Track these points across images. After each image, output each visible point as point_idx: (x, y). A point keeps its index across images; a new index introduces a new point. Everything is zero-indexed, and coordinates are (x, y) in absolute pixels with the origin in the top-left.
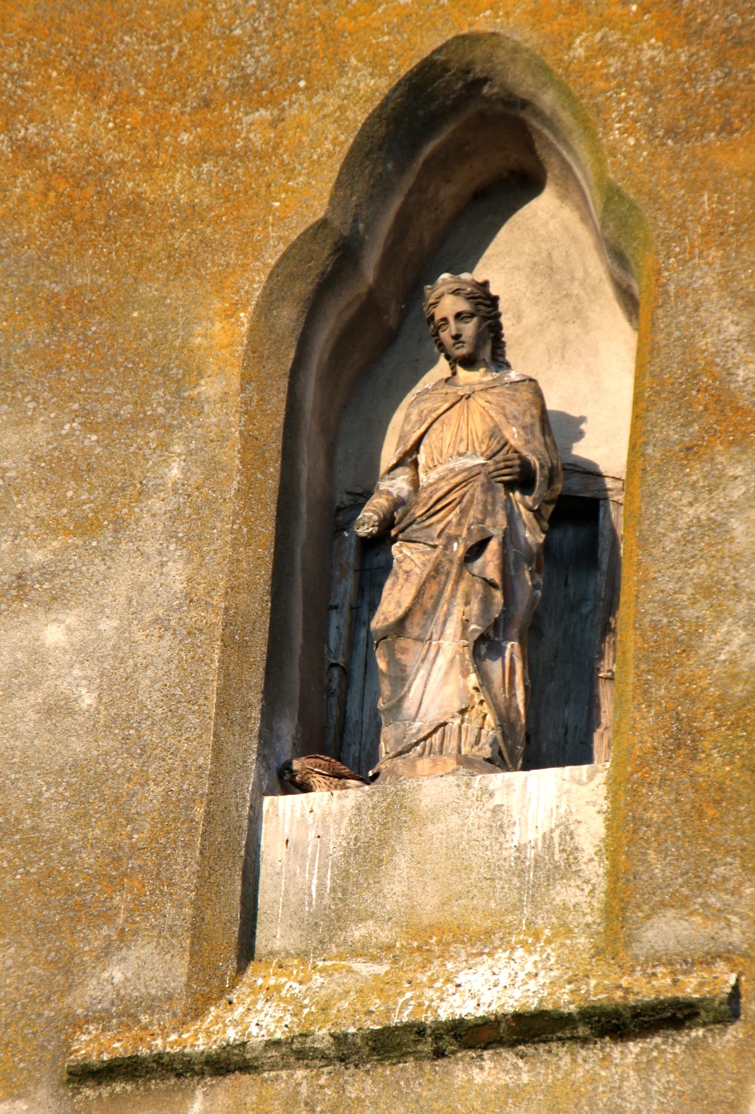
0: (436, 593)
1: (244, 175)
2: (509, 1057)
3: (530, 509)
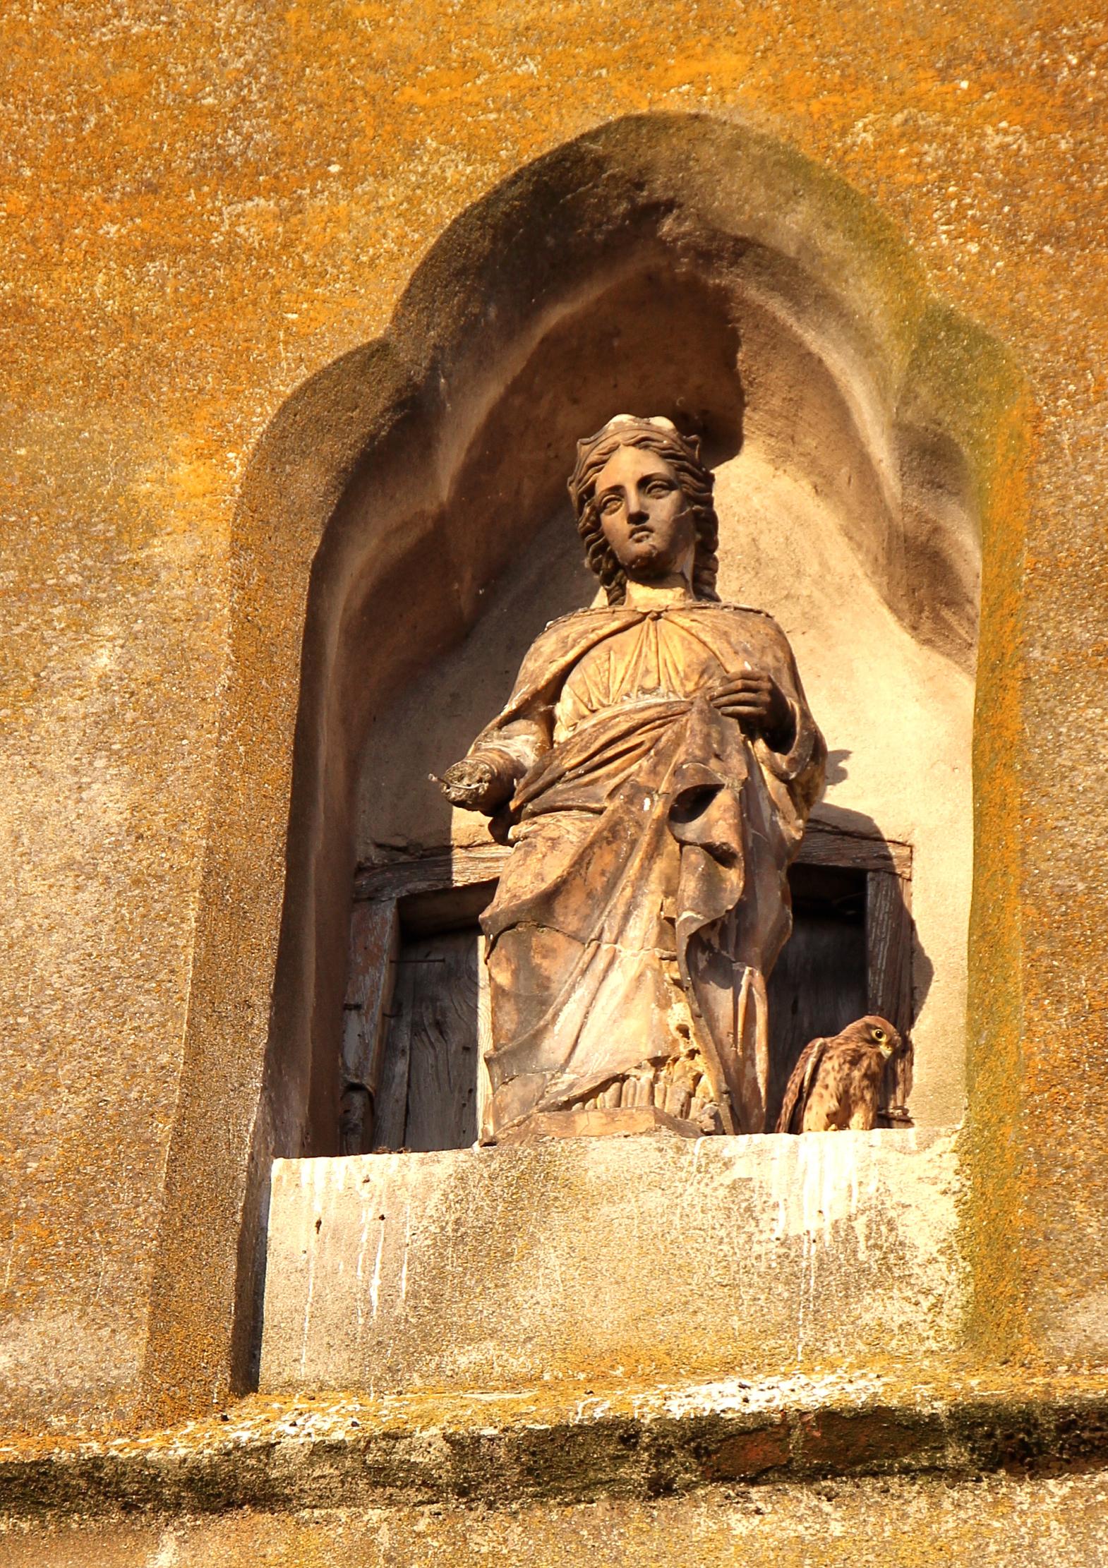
0: (611, 868)
1: (227, 278)
2: (804, 1498)
3: (781, 776)
